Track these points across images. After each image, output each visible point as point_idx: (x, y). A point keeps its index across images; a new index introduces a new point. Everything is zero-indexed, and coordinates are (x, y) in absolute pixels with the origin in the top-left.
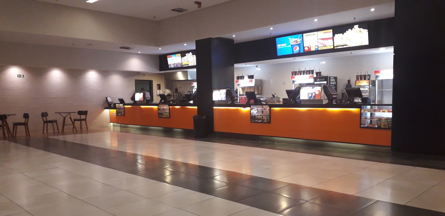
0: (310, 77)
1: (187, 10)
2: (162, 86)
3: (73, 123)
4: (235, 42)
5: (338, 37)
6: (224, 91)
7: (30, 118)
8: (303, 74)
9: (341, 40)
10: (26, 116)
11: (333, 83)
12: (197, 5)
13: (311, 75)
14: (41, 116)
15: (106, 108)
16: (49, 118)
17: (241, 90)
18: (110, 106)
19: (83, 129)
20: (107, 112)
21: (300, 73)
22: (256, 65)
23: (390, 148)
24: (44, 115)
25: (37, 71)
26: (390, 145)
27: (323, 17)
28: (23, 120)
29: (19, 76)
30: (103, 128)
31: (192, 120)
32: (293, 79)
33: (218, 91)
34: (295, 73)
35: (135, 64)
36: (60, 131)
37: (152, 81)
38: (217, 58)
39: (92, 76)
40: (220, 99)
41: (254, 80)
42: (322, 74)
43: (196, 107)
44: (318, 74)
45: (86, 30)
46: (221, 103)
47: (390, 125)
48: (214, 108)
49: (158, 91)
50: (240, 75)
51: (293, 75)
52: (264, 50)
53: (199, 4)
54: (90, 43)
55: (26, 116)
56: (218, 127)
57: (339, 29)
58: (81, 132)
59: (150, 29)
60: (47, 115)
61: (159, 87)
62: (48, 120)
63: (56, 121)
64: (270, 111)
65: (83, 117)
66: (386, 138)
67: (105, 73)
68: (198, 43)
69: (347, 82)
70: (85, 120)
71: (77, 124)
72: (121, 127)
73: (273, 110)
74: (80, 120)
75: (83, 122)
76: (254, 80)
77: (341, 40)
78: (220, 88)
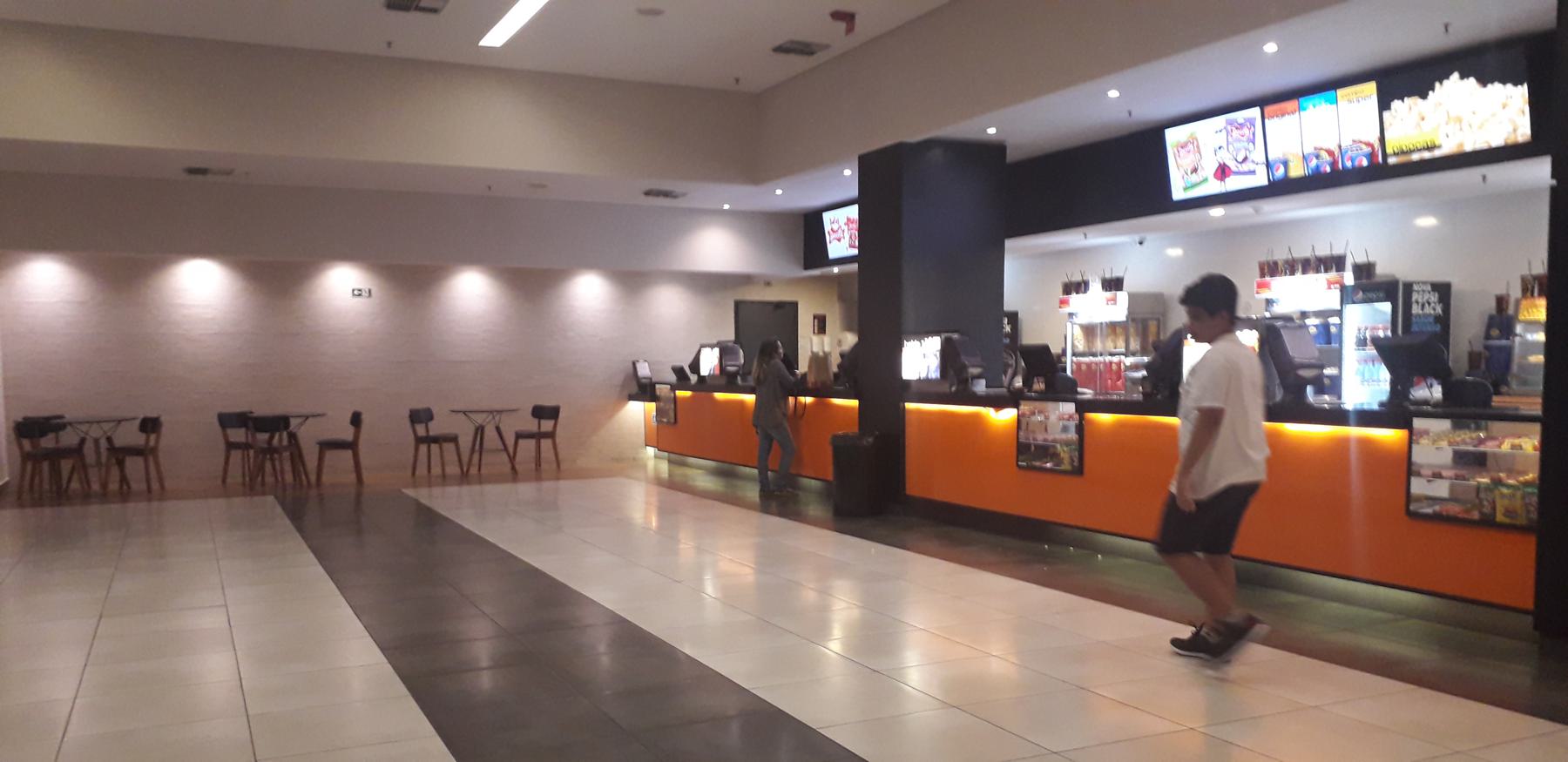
0: (1330, 283)
1: (827, 47)
2: (833, 323)
3: (121, 464)
4: (1011, 156)
5: (1403, 109)
6: (934, 344)
7: (164, 430)
8: (1304, 272)
9: (1422, 123)
10: (356, 420)
11: (1428, 310)
12: (842, 26)
13: (1333, 275)
14: (408, 423)
15: (632, 398)
16: (436, 428)
17: (1078, 333)
18: (645, 391)
19: (544, 466)
20: (638, 412)
21: (1291, 267)
22: (1137, 238)
23: (1530, 619)
24: (420, 417)
25: (276, 275)
26: (1530, 605)
27: (1299, 26)
28: (347, 434)
29: (358, 293)
30: (622, 464)
31: (829, 450)
32: (1266, 294)
33: (916, 343)
34: (1270, 269)
35: (716, 248)
36: (96, 487)
37: (795, 305)
38: (953, 212)
39: (588, 293)
40: (923, 376)
41: (1122, 297)
42: (1379, 270)
43: (854, 403)
44: (1364, 271)
45: (502, 140)
46: (925, 391)
47: (1534, 516)
48: (909, 406)
49: (815, 339)
50: (1077, 278)
51: (1263, 275)
52: (1120, 177)
53: (846, 18)
54: (537, 183)
55: (356, 420)
56: (917, 483)
57: (1403, 79)
58: (537, 473)
59: (719, 123)
60: (431, 418)
61: (821, 325)
62: (431, 433)
63: (454, 439)
64: (1080, 429)
65: (547, 425)
66: (1512, 572)
67: (631, 281)
68: (869, 167)
69: (1491, 305)
70: (551, 435)
71: (527, 446)
72: (670, 461)
73: (1092, 422)
74: (538, 436)
75: (546, 444)
76: (1122, 297)
77: (1422, 123)
78: (921, 333)
